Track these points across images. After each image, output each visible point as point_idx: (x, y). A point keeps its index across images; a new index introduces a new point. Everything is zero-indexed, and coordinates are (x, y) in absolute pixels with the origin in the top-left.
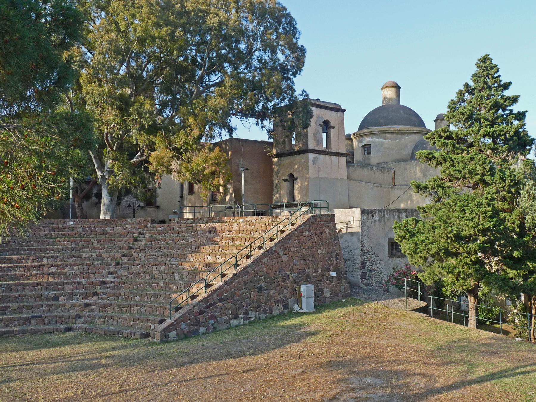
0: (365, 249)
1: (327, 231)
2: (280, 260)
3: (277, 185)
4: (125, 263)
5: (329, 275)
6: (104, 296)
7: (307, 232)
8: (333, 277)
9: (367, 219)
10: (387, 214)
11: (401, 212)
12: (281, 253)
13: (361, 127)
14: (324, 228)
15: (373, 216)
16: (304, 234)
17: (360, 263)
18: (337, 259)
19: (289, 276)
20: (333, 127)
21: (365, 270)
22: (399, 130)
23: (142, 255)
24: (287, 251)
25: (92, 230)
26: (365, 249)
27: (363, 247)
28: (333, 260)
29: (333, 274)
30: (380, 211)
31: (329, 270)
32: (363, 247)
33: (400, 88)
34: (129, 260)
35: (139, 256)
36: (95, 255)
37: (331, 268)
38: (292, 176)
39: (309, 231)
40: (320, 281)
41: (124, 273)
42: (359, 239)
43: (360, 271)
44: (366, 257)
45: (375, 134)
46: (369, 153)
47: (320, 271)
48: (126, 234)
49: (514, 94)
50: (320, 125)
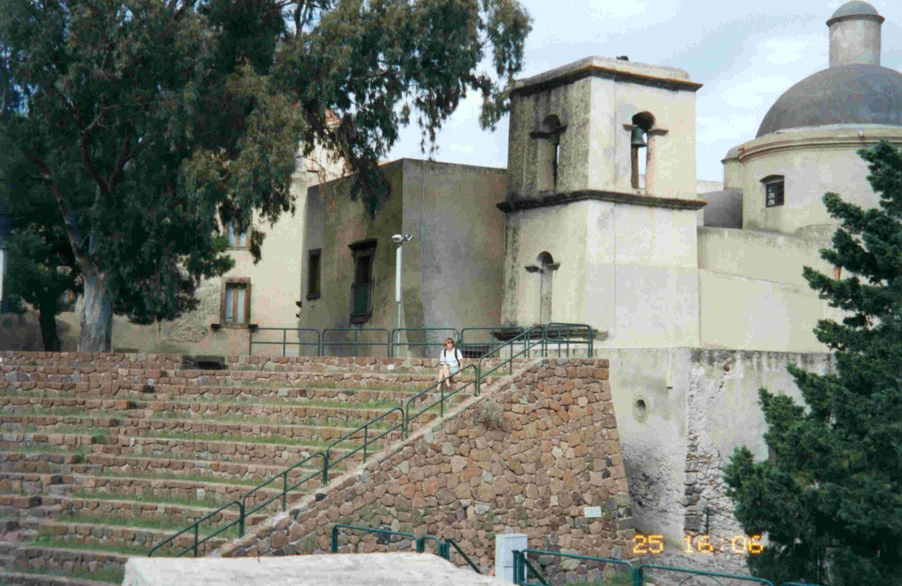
0: (699, 452)
1: (583, 401)
2: (445, 468)
3: (512, 280)
4: (98, 459)
5: (581, 514)
6: (34, 532)
7: (524, 401)
8: (591, 521)
9: (708, 375)
10: (769, 365)
11: (812, 362)
12: (447, 449)
13: (761, 132)
14: (575, 393)
15: (726, 369)
16: (515, 407)
17: (683, 488)
18: (606, 475)
19: (465, 508)
20: (663, 133)
21: (699, 507)
22: (863, 138)
23: (136, 442)
24: (464, 447)
25: (38, 378)
26: (699, 452)
27: (693, 447)
28: (596, 477)
29: (592, 512)
30: (748, 355)
31: (579, 501)
32: (693, 447)
33: (881, 20)
34: (107, 451)
35: (132, 443)
36: (31, 435)
37: (587, 497)
38: (546, 258)
39: (533, 399)
40: (554, 526)
41: (88, 480)
42: (683, 429)
43: (684, 511)
44: (700, 475)
45: (827, 145)
46: (780, 200)
47: (554, 501)
48: (114, 389)
49: (454, 114)
50: (627, 127)
